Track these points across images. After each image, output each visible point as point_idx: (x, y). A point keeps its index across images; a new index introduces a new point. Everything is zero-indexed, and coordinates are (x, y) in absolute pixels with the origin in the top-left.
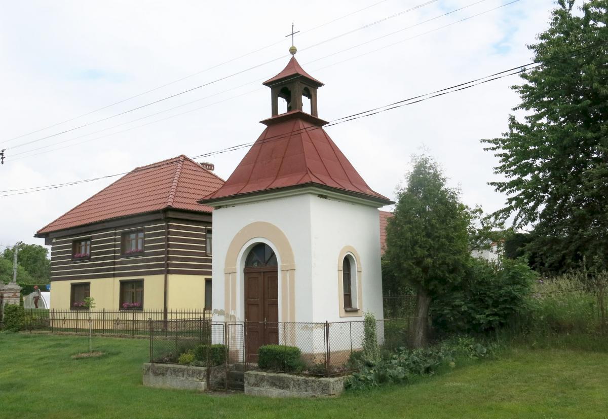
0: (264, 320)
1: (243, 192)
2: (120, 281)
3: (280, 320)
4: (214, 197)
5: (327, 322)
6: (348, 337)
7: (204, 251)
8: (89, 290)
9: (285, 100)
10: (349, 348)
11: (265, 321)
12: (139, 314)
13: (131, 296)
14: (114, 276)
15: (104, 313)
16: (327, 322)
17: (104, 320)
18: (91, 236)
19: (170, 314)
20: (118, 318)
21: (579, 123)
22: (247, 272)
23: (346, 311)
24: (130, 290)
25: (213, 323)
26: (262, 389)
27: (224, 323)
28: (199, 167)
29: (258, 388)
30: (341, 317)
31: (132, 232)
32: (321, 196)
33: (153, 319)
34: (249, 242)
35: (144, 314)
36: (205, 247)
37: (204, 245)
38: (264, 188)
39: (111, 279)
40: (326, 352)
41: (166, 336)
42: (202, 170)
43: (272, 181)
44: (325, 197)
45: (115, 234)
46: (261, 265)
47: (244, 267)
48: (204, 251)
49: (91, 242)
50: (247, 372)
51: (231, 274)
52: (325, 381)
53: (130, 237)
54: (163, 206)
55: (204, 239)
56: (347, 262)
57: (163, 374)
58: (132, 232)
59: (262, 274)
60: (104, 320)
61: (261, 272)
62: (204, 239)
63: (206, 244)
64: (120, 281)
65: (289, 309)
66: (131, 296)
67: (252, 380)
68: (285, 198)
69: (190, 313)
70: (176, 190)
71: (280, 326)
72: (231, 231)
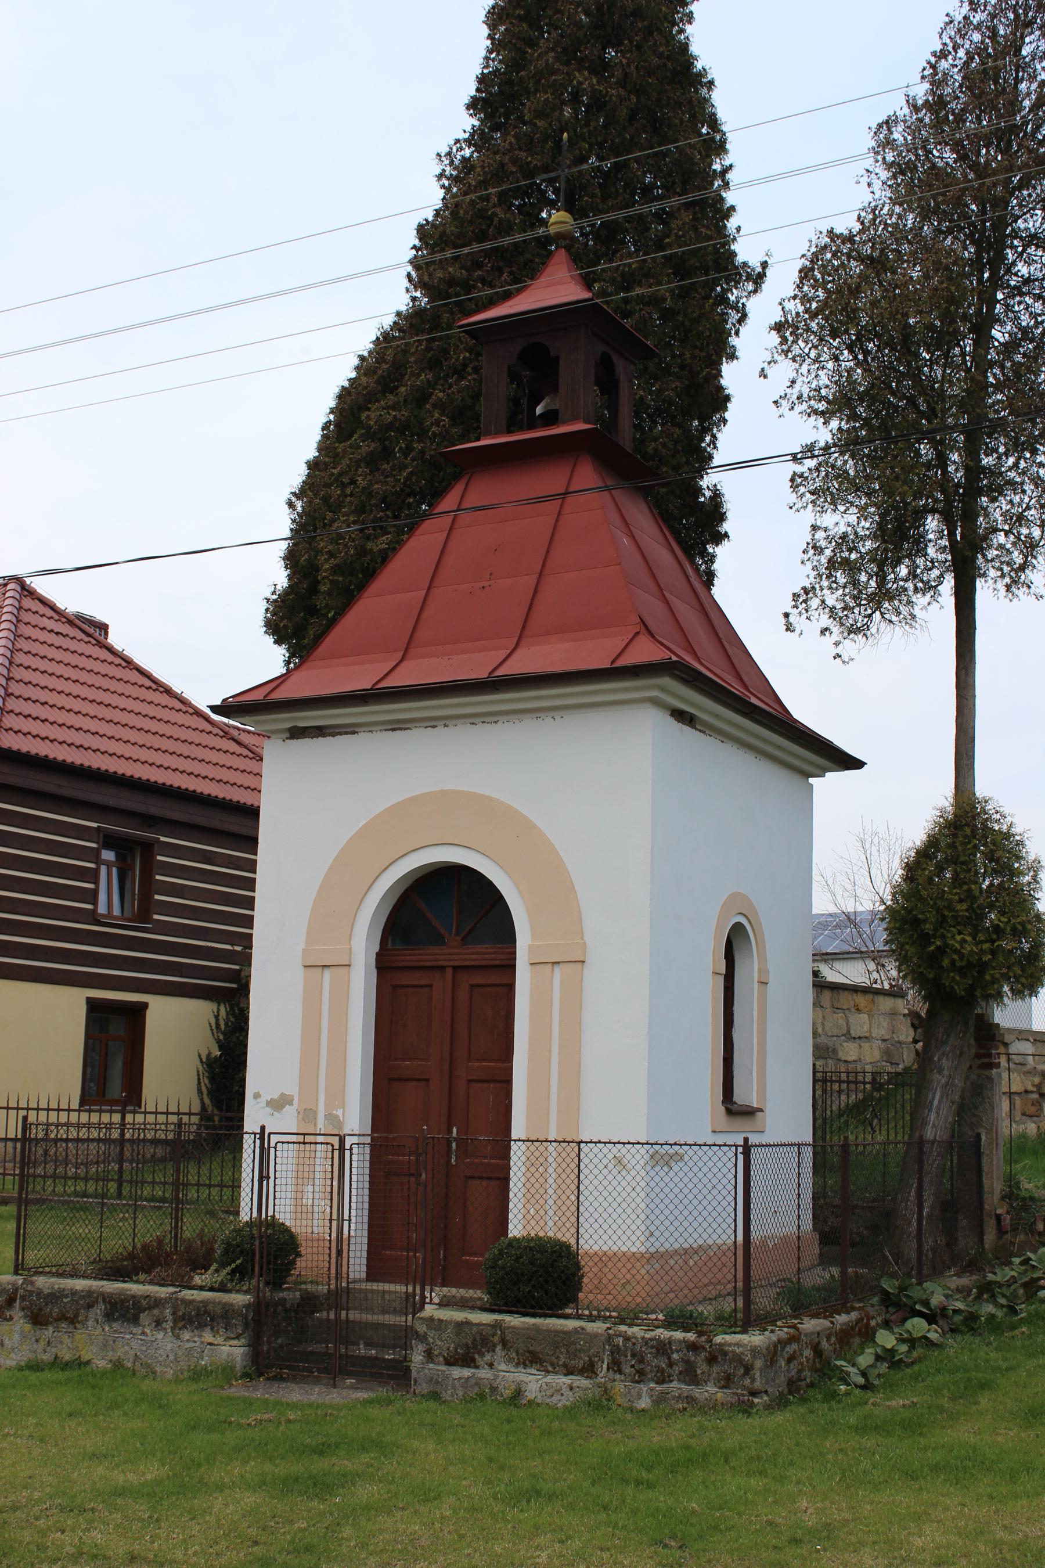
1: (394, 681)
3: (518, 1128)
4: (277, 695)
7: (90, 907)
22: (385, 965)
26: (484, 1373)
27: (335, 1141)
29: (467, 1372)
30: (714, 1132)
32: (681, 716)
36: (95, 893)
37: (91, 886)
38: (480, 673)
41: (746, 1140)
42: (80, 635)
43: (504, 653)
46: (447, 939)
47: (376, 948)
48: (90, 907)
52: (738, 1345)
55: (92, 865)
56: (734, 943)
57: (73, 1321)
59: (449, 971)
61: (442, 968)
62: (92, 865)
63: (96, 882)
65: (554, 1090)
67: (443, 1344)
68: (557, 715)
69: (38, 1109)
70: (6, 689)
71: (518, 1153)
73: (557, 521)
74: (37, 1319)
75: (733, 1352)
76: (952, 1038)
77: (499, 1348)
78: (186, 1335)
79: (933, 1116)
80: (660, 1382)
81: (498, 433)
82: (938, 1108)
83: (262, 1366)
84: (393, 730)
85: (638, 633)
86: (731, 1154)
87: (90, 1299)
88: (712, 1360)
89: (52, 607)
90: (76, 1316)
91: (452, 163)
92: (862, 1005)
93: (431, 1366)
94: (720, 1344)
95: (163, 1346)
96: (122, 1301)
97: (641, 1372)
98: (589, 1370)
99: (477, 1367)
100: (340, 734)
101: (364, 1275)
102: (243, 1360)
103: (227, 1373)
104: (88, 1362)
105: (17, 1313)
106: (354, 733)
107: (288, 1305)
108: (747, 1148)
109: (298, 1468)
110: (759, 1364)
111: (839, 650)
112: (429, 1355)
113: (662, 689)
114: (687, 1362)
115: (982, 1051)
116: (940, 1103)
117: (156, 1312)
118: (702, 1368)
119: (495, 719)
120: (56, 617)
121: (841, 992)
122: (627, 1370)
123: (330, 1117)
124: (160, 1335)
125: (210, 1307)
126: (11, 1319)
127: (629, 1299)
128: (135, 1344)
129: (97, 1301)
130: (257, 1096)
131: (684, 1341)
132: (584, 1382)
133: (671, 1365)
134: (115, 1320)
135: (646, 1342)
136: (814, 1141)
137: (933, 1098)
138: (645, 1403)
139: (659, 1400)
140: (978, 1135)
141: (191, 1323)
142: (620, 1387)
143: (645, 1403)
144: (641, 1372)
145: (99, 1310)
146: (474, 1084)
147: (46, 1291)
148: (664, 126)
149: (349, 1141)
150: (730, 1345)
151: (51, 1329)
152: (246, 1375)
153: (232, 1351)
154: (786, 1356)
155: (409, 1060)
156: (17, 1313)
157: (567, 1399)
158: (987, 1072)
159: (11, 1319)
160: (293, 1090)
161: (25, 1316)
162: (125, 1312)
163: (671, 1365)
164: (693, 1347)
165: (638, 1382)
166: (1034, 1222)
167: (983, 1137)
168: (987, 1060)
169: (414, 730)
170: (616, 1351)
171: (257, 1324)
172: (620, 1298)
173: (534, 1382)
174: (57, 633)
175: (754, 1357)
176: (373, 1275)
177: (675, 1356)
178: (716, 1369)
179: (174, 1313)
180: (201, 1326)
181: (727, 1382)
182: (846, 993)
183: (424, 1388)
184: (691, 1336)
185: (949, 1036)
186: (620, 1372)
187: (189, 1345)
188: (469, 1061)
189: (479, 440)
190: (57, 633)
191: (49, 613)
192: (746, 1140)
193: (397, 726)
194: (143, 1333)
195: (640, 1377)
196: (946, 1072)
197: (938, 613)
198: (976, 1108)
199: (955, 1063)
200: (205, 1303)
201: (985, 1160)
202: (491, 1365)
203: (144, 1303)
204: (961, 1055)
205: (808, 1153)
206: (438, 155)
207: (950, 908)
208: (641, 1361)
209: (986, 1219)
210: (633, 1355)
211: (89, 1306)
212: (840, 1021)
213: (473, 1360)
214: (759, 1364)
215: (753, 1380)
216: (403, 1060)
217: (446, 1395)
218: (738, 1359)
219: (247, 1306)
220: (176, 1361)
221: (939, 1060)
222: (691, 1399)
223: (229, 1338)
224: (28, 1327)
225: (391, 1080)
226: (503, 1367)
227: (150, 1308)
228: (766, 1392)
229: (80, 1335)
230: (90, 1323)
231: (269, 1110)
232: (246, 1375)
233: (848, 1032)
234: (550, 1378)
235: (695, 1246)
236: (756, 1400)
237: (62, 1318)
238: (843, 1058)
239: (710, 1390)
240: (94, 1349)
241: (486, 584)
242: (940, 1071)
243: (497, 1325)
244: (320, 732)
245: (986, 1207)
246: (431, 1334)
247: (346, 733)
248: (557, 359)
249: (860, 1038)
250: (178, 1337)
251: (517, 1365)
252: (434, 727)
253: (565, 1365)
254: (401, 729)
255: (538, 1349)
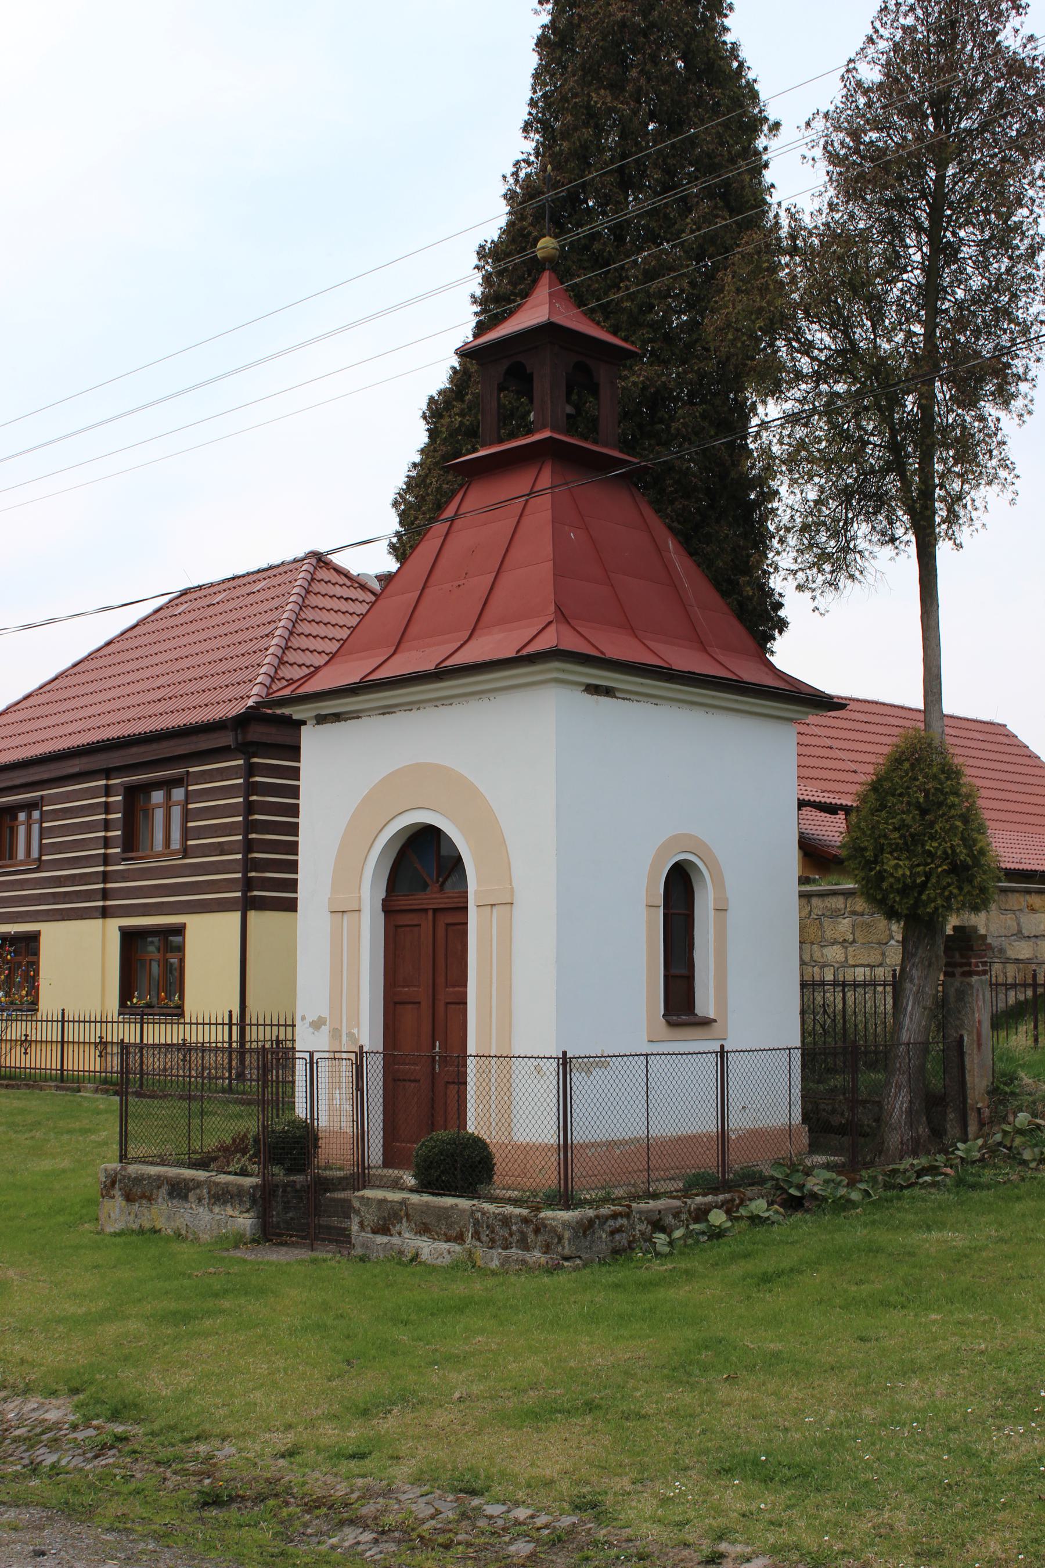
0: (434, 1047)
2: (121, 928)
5: (565, 1053)
6: (660, 1100)
8: (36, 953)
9: (423, 439)
10: (642, 1133)
11: (437, 1049)
12: (175, 1026)
13: (150, 969)
14: (105, 913)
15: (63, 1021)
16: (565, 1053)
17: (63, 1042)
18: (42, 797)
19: (71, 1024)
20: (101, 1038)
21: (827, 567)
22: (389, 908)
23: (670, 1024)
24: (152, 949)
25: (298, 1055)
26: (396, 1240)
28: (363, 587)
31: (157, 785)
33: (126, 1041)
34: (400, 817)
35: (39, 1023)
38: (429, 666)
39: (95, 925)
40: (562, 1142)
41: (722, 1047)
44: (608, 692)
45: (108, 791)
49: (42, 813)
50: (361, 1193)
51: (346, 916)
52: (553, 1219)
53: (149, 798)
54: (237, 709)
56: (680, 885)
57: (150, 1199)
58: (157, 785)
59: (430, 913)
60: (63, 1042)
61: (426, 910)
63: (41, 845)
64: (121, 928)
66: (150, 969)
67: (371, 1217)
71: (471, 1063)
72: (347, 790)
73: (518, 522)
74: (129, 1198)
75: (551, 1224)
76: (920, 951)
77: (404, 1220)
78: (216, 1210)
79: (907, 1021)
80: (505, 1248)
81: (491, 444)
82: (911, 1014)
83: (268, 1234)
84: (384, 714)
85: (551, 622)
86: (555, 1065)
87: (159, 1181)
88: (537, 1231)
89: (347, 575)
90: (151, 1195)
91: (517, 181)
92: (1036, 906)
93: (363, 1234)
94: (542, 1219)
95: (203, 1218)
96: (178, 1183)
97: (493, 1240)
98: (460, 1238)
99: (391, 1235)
100: (350, 719)
101: (380, 1162)
102: (251, 1229)
103: (239, 1241)
104: (160, 1230)
105: (117, 1192)
106: (358, 717)
107: (298, 1187)
108: (722, 1053)
109: (173, 1306)
110: (567, 1234)
111: (816, 604)
112: (361, 1224)
113: (558, 670)
114: (522, 1232)
115: (964, 961)
116: (912, 1009)
117: (198, 1191)
118: (531, 1237)
119: (450, 701)
120: (349, 583)
121: (1010, 894)
122: (484, 1238)
123: (350, 1035)
124: (201, 1210)
125: (230, 1188)
126: (113, 1197)
127: (544, 1181)
128: (187, 1216)
129: (163, 1184)
130: (303, 1018)
131: (520, 1215)
132: (457, 1248)
133: (511, 1235)
134: (174, 1198)
135: (496, 1215)
136: (803, 1042)
137: (907, 1005)
138: (495, 1264)
139: (505, 1261)
140: (962, 1036)
141: (219, 1200)
142: (479, 1252)
143: (495, 1264)
144: (493, 1240)
145: (164, 1190)
146: (449, 1006)
147: (133, 1176)
148: (722, 108)
149: (316, 1056)
150: (548, 1219)
151: (137, 1205)
152: (254, 1241)
153: (245, 1222)
154: (608, 1229)
155: (408, 986)
156: (117, 1192)
157: (447, 1260)
158: (968, 980)
159: (113, 1197)
160: (325, 1014)
161: (122, 1195)
162: (179, 1190)
163: (511, 1235)
164: (526, 1221)
165: (491, 1248)
166: (1006, 1115)
167: (966, 1039)
168: (966, 969)
169: (399, 714)
170: (477, 1223)
171: (263, 1200)
172: (538, 1180)
173: (428, 1248)
174: (346, 599)
175: (564, 1229)
176: (387, 1163)
177: (514, 1228)
178: (540, 1238)
179: (209, 1193)
180: (225, 1203)
181: (547, 1249)
182: (1017, 895)
183: (358, 1251)
184: (525, 1212)
185: (917, 949)
186: (479, 1240)
187: (218, 1217)
188: (446, 987)
189: (475, 450)
190: (346, 599)
191: (342, 580)
192: (722, 1047)
193: (386, 711)
194: (191, 1208)
195: (492, 1244)
196: (916, 981)
197: (905, 563)
198: (959, 1012)
199: (925, 972)
200: (227, 1184)
201: (967, 1059)
202: (400, 1234)
203: (191, 1184)
204: (930, 965)
205: (797, 1055)
206: (504, 177)
207: (886, 836)
208: (492, 1232)
209: (969, 1112)
210: (488, 1227)
211: (159, 1187)
212: (1009, 922)
213: (389, 1230)
214: (567, 1234)
215: (564, 1248)
216: (404, 987)
217: (373, 1257)
218: (553, 1230)
219: (255, 1187)
220: (211, 1230)
221: (911, 970)
222: (524, 1262)
223: (241, 1212)
224: (124, 1203)
225: (396, 1003)
226: (407, 1235)
227: (194, 1189)
228: (579, 1257)
229: (155, 1209)
230: (160, 1200)
231: (311, 1030)
232: (254, 1241)
233: (1020, 931)
234: (436, 1244)
235: (627, 1138)
236: (566, 1264)
237: (143, 1196)
238: (1013, 957)
239: (536, 1256)
240: (163, 1220)
241: (460, 583)
242: (912, 981)
243: (403, 1202)
244: (337, 717)
245: (969, 1101)
246: (363, 1209)
247: (353, 718)
248: (532, 374)
249: (1036, 937)
250: (211, 1211)
251: (416, 1233)
252: (411, 710)
253: (445, 1234)
254: (389, 713)
255: (428, 1221)
